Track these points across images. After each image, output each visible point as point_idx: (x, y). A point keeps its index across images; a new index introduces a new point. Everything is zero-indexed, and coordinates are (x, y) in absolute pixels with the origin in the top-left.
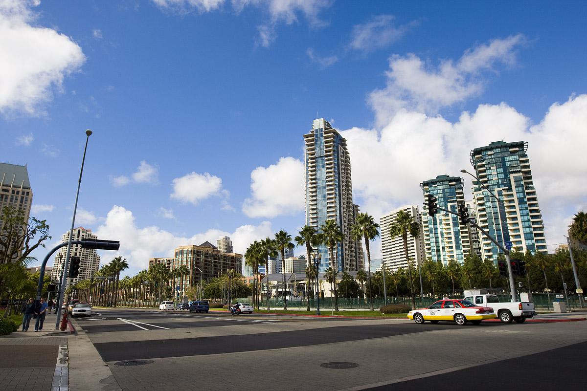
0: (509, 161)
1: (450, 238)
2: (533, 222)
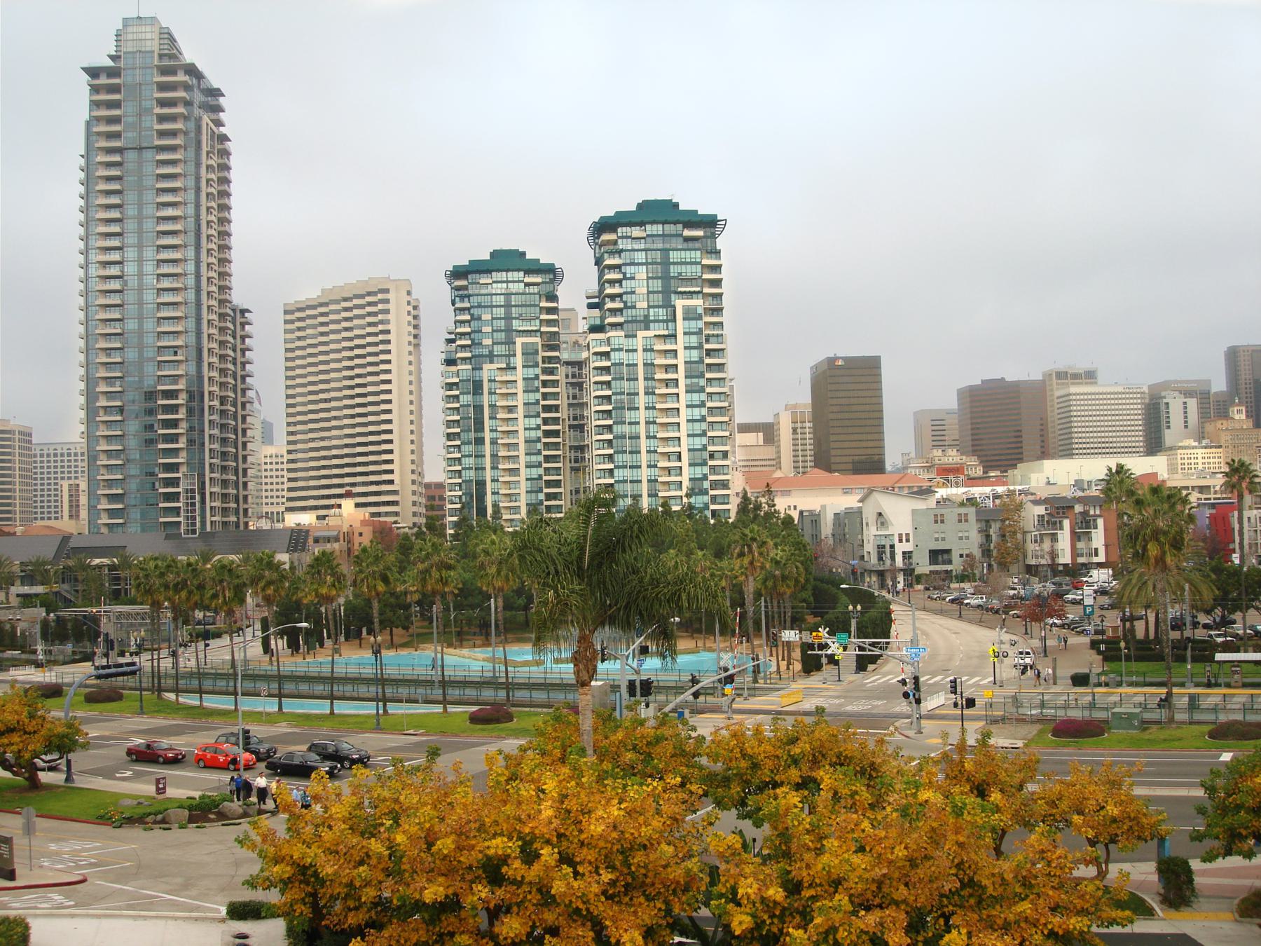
0: (677, 263)
1: (514, 472)
2: (709, 380)
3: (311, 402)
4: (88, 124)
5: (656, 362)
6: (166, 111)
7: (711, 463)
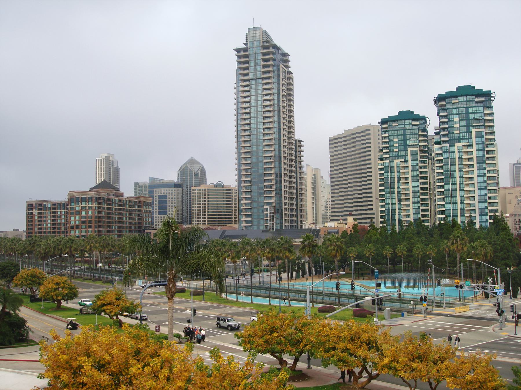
2: (488, 164)
3: (340, 177)
4: (237, 71)
5: (463, 157)
6: (266, 63)
7: (489, 201)
